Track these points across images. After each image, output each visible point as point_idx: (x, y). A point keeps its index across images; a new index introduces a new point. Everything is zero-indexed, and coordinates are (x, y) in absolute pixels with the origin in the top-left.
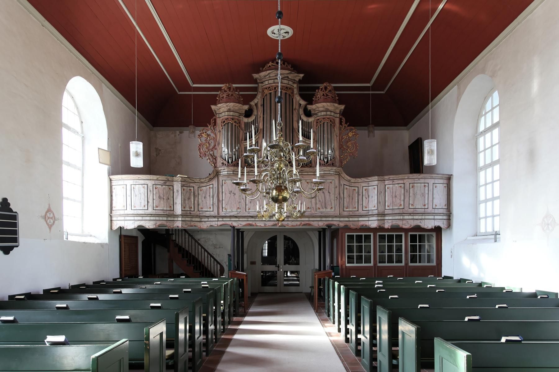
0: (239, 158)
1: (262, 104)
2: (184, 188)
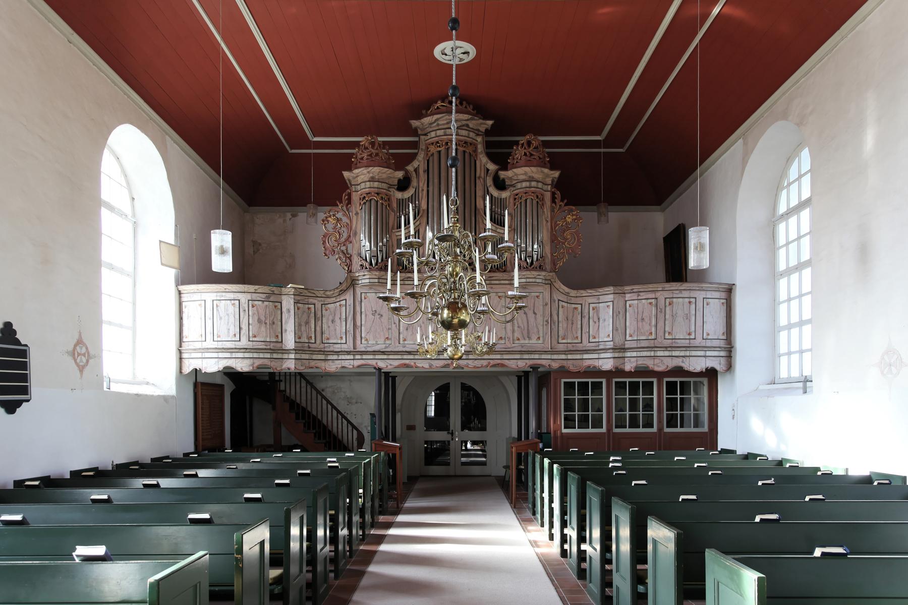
0: (389, 257)
1: (426, 169)
2: (300, 305)
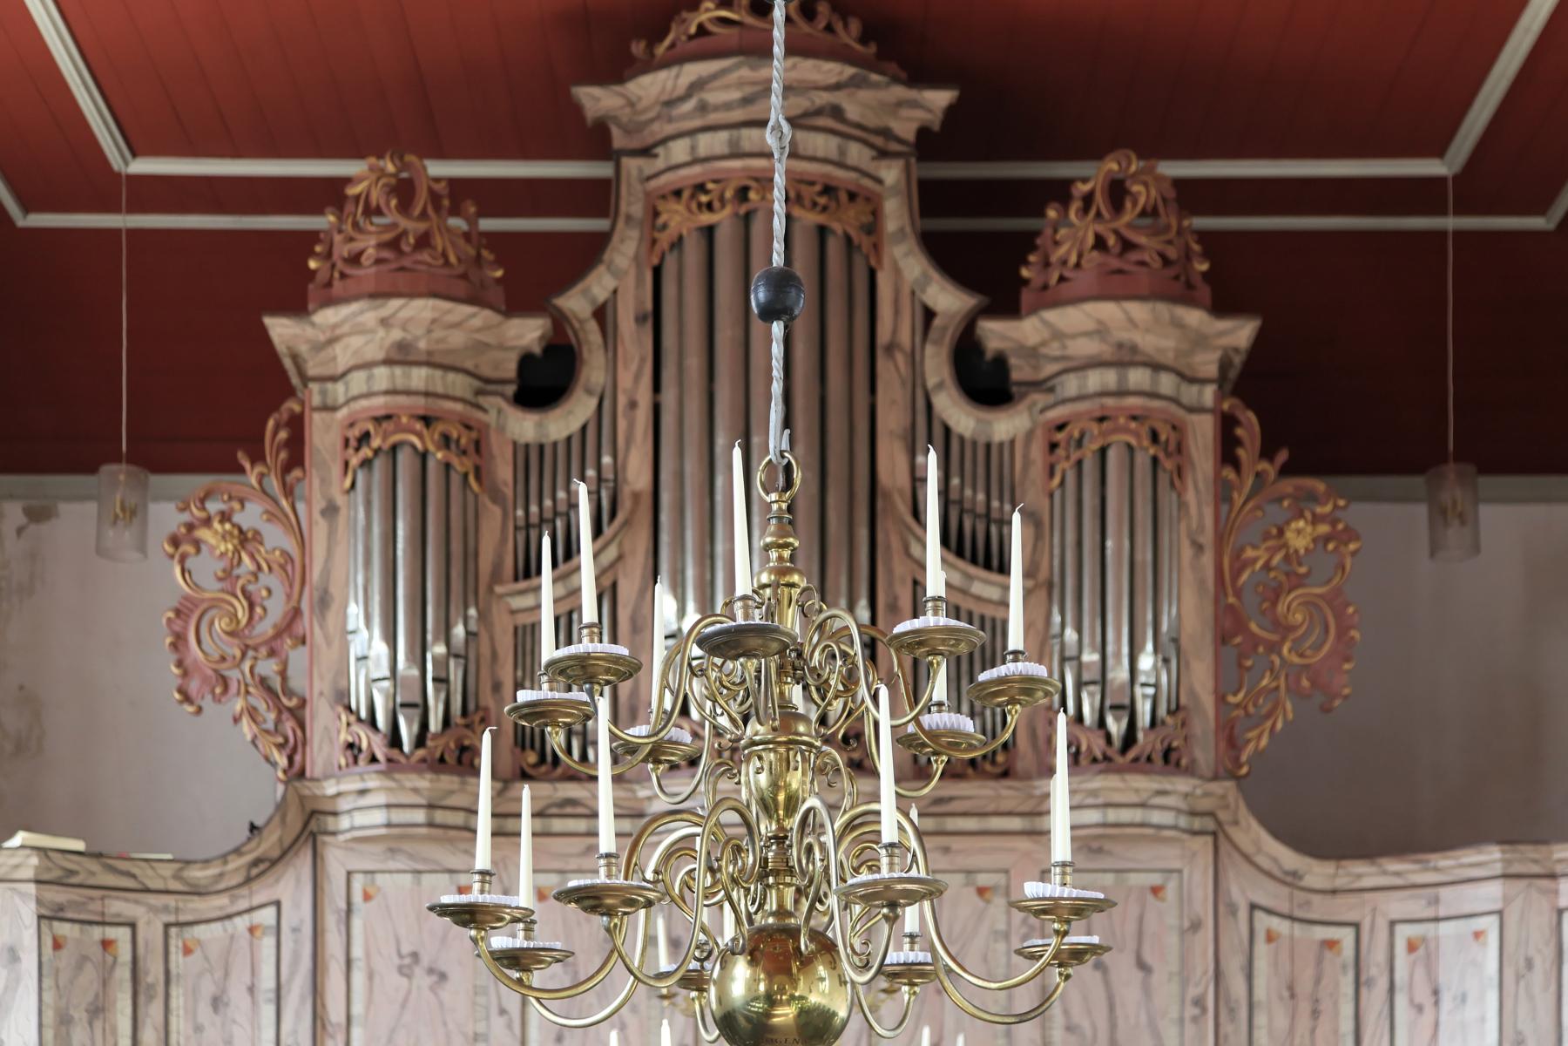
0: (485, 722)
2: (64, 929)
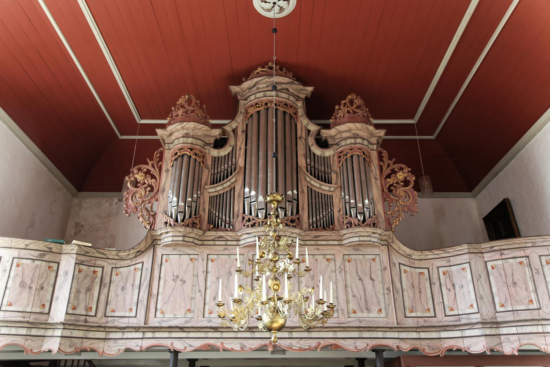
1: (245, 129)
